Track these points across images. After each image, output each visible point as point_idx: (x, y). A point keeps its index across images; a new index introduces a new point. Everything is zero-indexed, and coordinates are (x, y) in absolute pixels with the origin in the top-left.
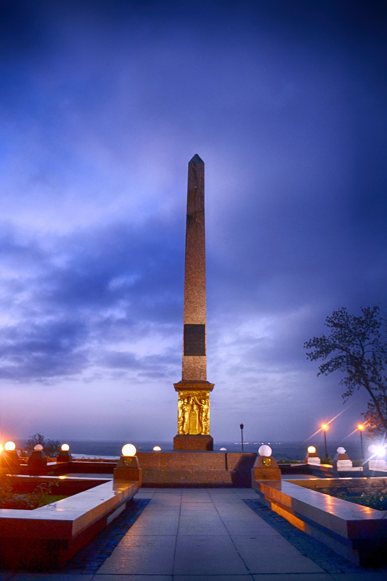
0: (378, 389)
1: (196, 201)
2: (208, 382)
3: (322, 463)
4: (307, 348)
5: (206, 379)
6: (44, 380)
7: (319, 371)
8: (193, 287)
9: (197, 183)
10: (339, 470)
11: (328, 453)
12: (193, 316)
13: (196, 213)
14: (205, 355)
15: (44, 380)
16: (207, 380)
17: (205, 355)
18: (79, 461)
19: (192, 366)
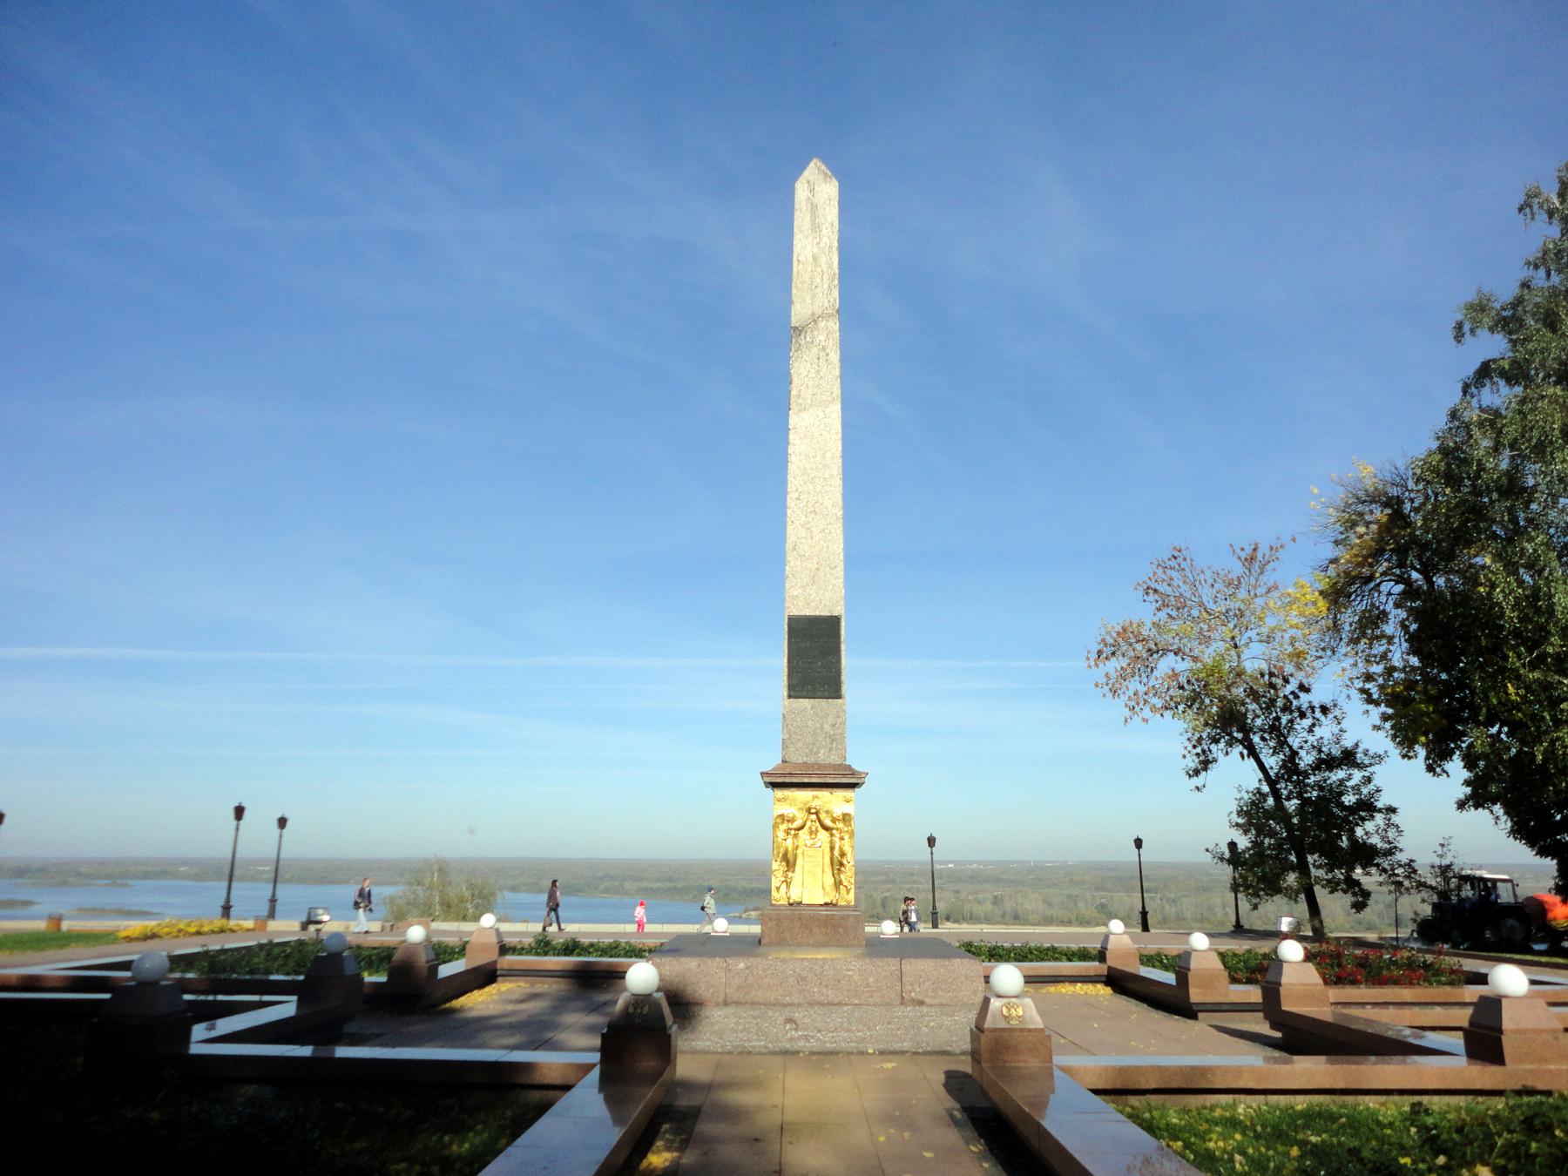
0: (1317, 706)
1: (816, 287)
2: (850, 766)
3: (1540, 1164)
4: (1097, 666)
5: (845, 760)
6: (1148, 960)
7: (1127, 713)
8: (810, 519)
9: (818, 240)
10: (1261, 1001)
11: (1147, 910)
12: (810, 595)
13: (815, 321)
14: (839, 696)
15: (1148, 960)
16: (848, 763)
17: (839, 696)
18: (1470, 955)
19: (807, 726)
